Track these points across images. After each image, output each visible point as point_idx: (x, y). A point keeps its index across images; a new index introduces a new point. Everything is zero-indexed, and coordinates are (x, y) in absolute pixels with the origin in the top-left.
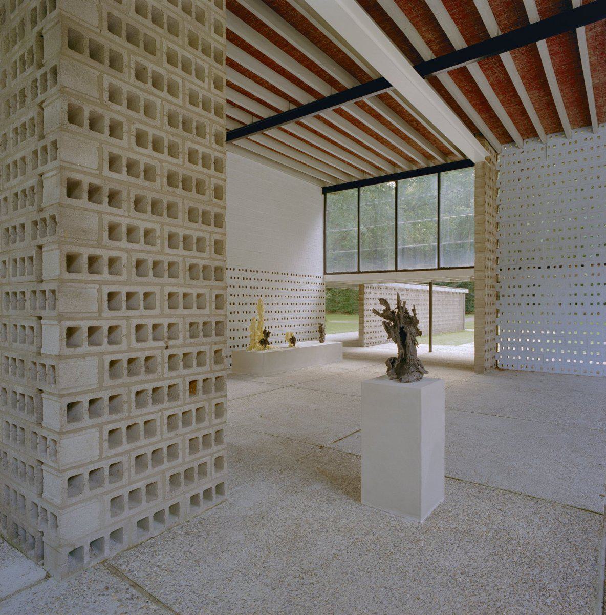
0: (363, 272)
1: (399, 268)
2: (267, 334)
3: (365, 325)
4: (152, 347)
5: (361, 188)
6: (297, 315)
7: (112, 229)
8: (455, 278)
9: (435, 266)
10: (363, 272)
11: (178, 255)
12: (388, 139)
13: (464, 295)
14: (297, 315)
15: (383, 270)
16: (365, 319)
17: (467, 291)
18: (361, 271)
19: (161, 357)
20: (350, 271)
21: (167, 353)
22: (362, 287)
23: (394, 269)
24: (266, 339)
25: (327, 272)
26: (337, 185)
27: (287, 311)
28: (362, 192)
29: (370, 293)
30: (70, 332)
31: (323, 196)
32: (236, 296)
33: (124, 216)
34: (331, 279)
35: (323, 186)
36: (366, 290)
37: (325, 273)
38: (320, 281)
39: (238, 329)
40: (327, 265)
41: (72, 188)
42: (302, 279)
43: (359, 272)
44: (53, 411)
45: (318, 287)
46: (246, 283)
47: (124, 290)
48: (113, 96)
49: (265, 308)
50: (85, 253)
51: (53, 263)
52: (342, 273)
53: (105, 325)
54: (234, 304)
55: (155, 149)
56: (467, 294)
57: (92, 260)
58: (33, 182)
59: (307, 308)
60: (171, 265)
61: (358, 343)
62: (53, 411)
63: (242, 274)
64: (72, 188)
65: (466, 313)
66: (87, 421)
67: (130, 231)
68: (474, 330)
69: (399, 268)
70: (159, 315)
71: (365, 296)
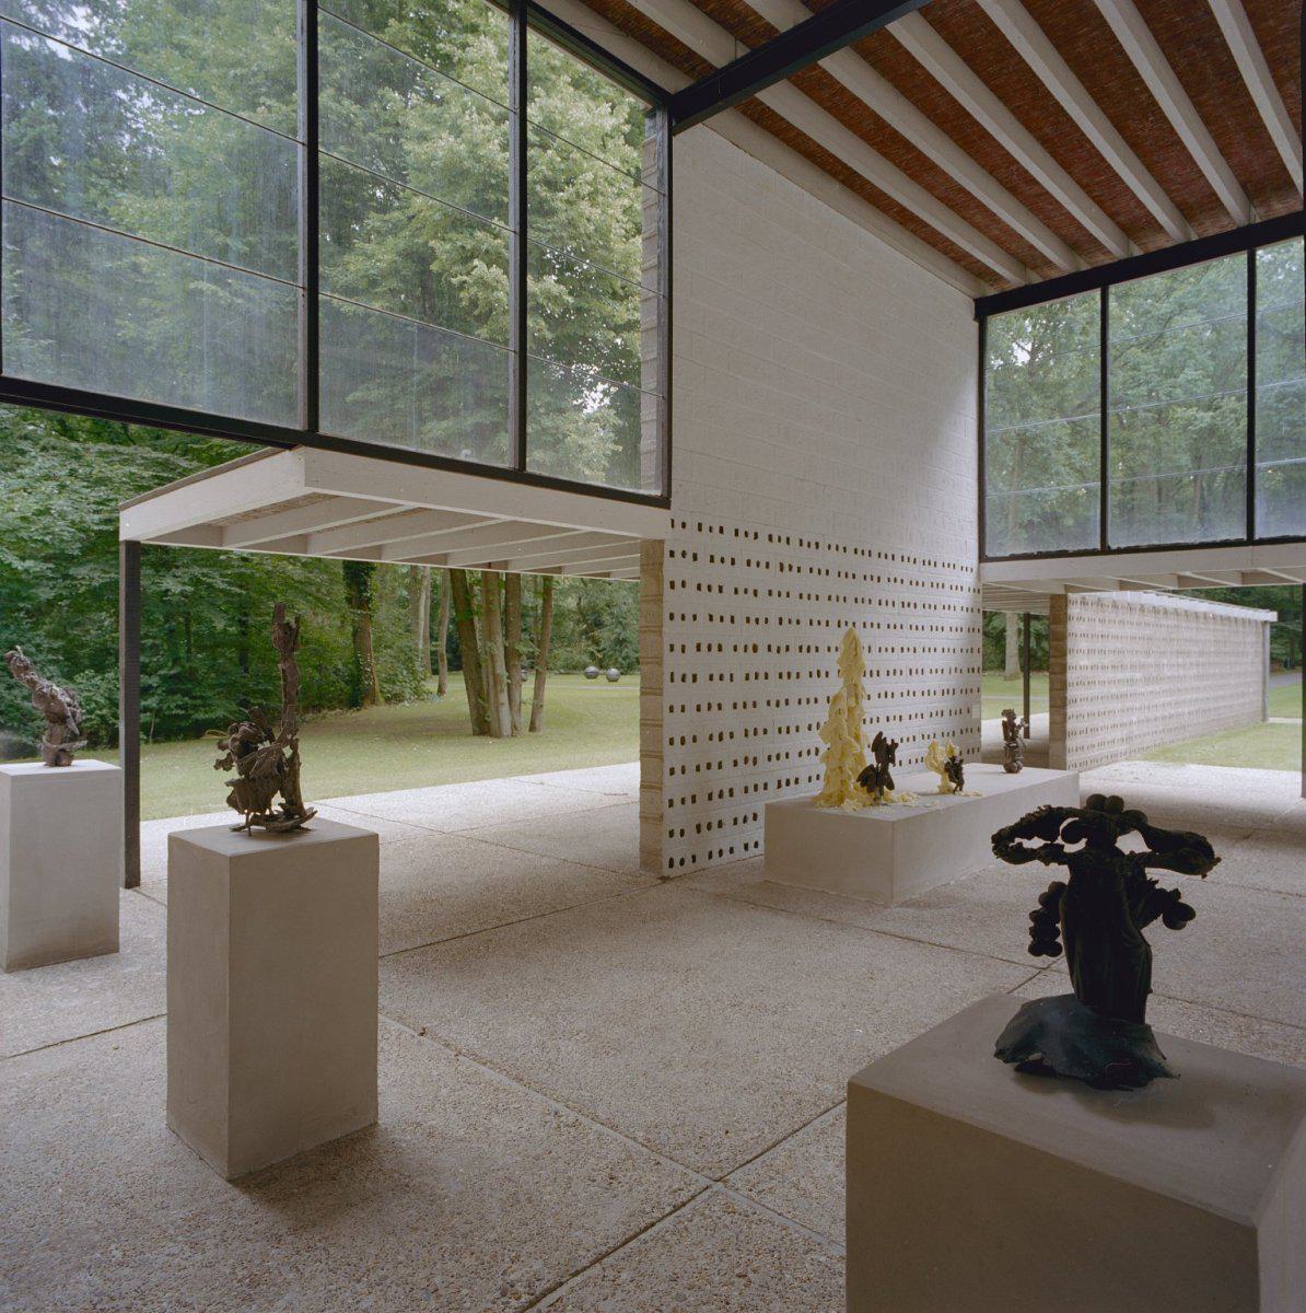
0: (1119, 551)
1: (1259, 534)
3: (1070, 710)
5: (1113, 289)
6: (916, 683)
8: (1216, 575)
10: (1119, 551)
12: (184, 545)
13: (1268, 626)
14: (916, 683)
15: (1197, 540)
16: (1071, 693)
17: (1272, 616)
18: (1114, 547)
20: (1071, 549)
22: (1059, 605)
23: (1244, 537)
24: (885, 769)
25: (989, 553)
26: (1001, 294)
27: (716, 677)
28: (1113, 304)
31: (976, 324)
32: (762, 621)
34: (997, 573)
35: (978, 296)
36: (1073, 610)
37: (982, 558)
38: (968, 579)
39: (765, 732)
42: (926, 574)
43: (1105, 550)
46: (789, 581)
54: (755, 649)
56: (1273, 625)
59: (938, 660)
63: (778, 552)
65: (1273, 671)
68: (1300, 721)
69: (1259, 534)
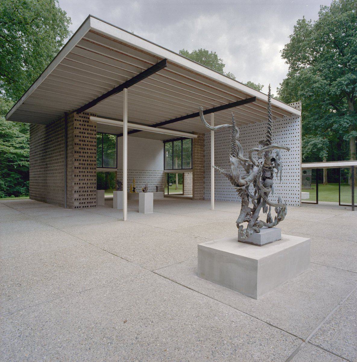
2: (134, 188)
4: (84, 185)
7: (80, 172)
9: (190, 167)
11: (89, 174)
19: (86, 187)
21: (87, 186)
29: (50, 180)
30: (75, 183)
33: (81, 170)
34: (166, 171)
37: (164, 170)
38: (162, 172)
40: (165, 166)
41: (75, 168)
42: (154, 172)
44: (73, 192)
45: (161, 174)
47: (89, 179)
48: (80, 156)
49: (135, 181)
50: (77, 175)
51: (73, 176)
52: (169, 169)
53: (79, 183)
55: (92, 150)
57: (77, 175)
58: (71, 167)
60: (87, 175)
61: (183, 194)
62: (73, 192)
64: (75, 168)
66: (77, 185)
67: (82, 171)
70: (86, 182)
71: (185, 177)
